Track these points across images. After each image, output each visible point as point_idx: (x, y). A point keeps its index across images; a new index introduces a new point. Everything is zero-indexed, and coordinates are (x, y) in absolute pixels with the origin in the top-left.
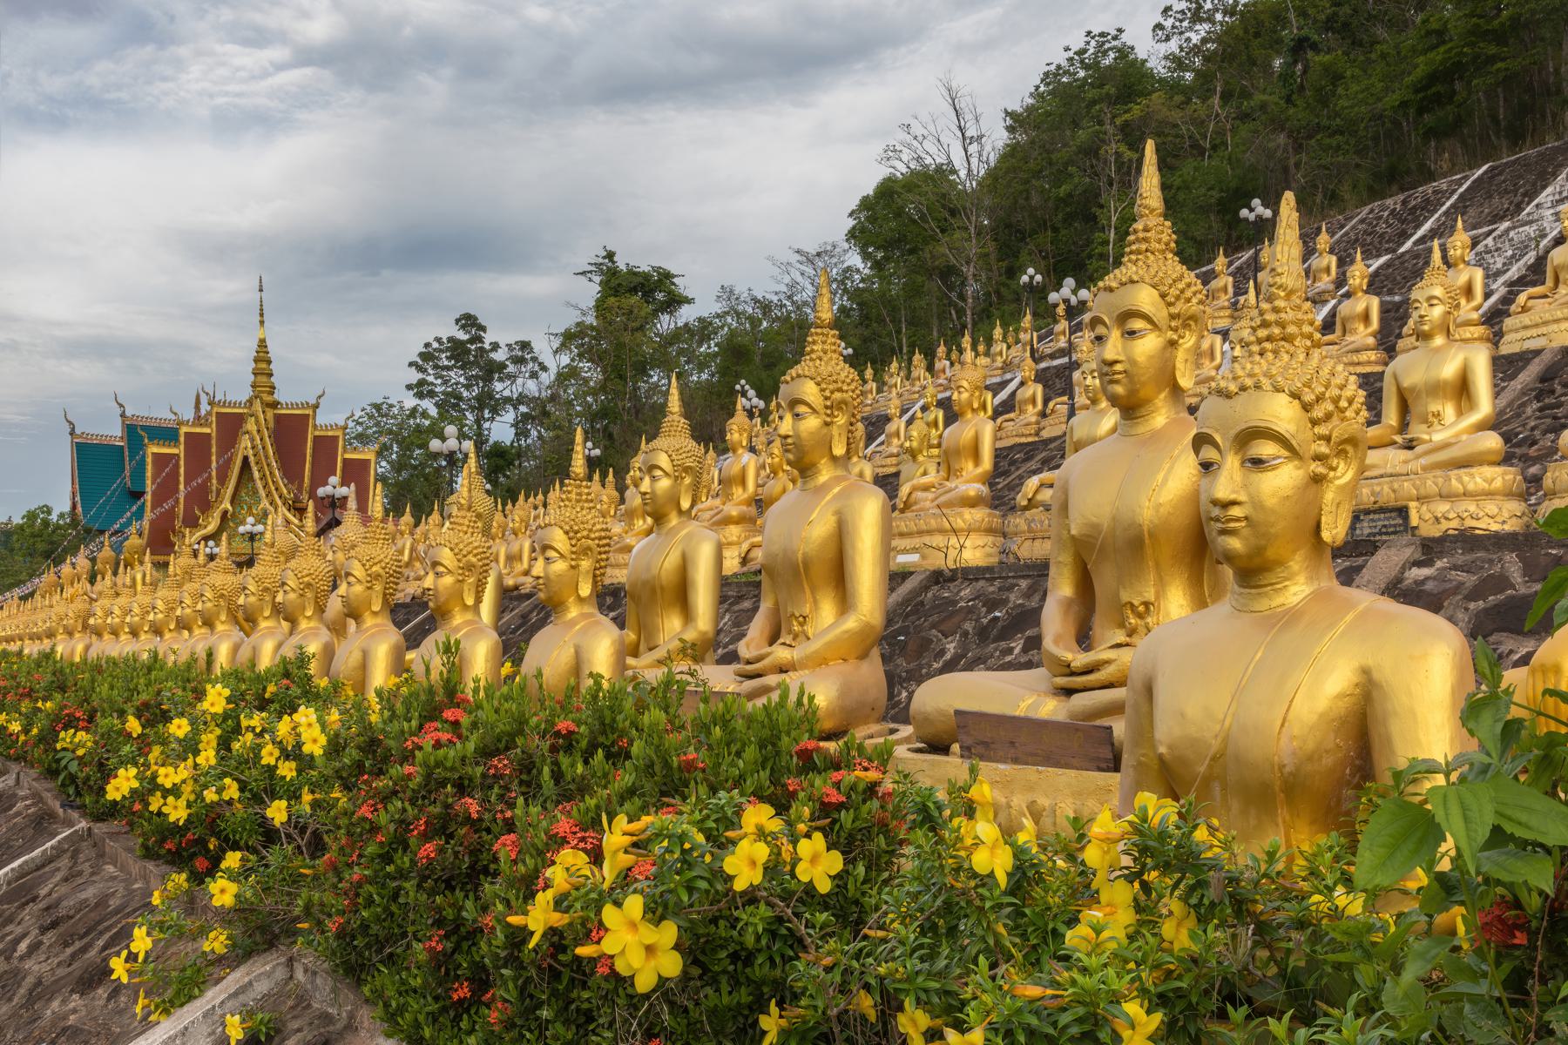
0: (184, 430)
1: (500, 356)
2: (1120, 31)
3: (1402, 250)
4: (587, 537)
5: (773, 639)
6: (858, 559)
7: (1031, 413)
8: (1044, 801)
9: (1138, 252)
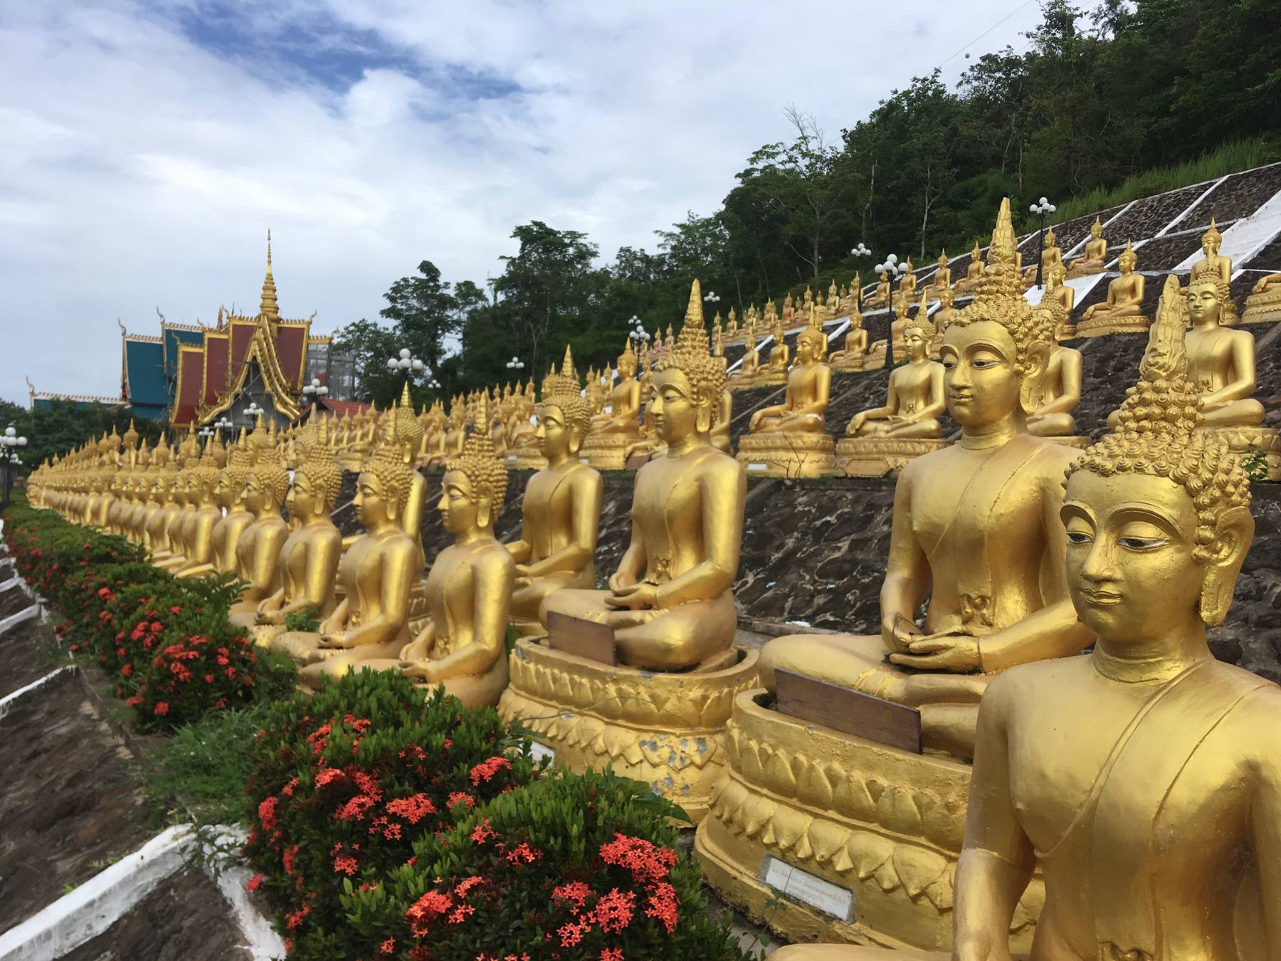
0: (207, 336)
1: (451, 292)
2: (937, 71)
3: (1158, 236)
4: (487, 480)
5: (640, 574)
6: (716, 520)
7: (857, 352)
8: (882, 781)
9: (990, 293)
